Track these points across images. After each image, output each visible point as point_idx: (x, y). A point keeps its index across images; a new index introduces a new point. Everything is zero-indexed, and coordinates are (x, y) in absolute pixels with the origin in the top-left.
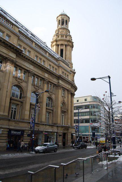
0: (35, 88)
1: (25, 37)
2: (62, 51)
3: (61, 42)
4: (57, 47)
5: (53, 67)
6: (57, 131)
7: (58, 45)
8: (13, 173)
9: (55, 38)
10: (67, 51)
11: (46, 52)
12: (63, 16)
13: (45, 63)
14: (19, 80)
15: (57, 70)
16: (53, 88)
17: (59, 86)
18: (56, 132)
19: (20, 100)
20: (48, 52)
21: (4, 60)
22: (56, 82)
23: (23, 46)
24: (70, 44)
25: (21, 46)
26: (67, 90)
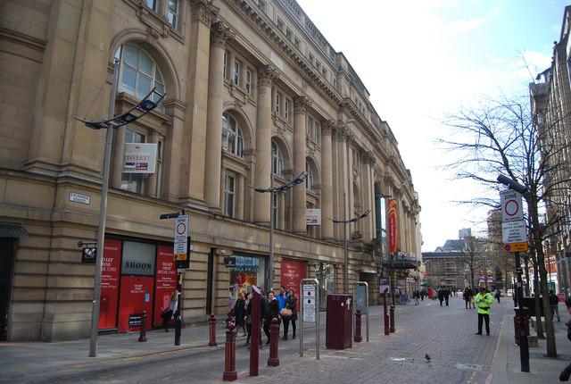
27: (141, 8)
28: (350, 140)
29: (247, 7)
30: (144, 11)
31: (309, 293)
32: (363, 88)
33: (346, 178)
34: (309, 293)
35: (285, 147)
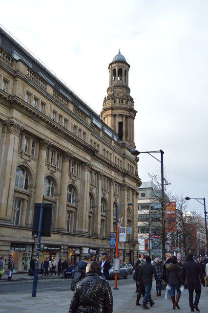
1: (35, 76)
2: (121, 124)
3: (119, 111)
4: (113, 118)
5: (60, 116)
6: (124, 248)
7: (114, 116)
8: (150, 290)
9: (109, 104)
10: (129, 127)
12: (121, 64)
13: (45, 108)
17: (12, 125)
18: (122, 250)
21: (36, 142)
23: (59, 112)
24: (131, 113)
25: (30, 95)
26: (132, 189)
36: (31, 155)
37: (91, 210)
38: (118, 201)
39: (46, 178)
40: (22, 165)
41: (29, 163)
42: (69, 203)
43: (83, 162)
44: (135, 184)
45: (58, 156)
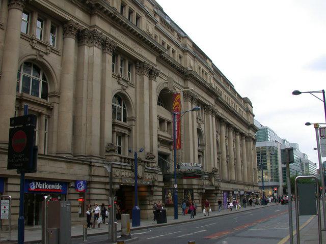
0: (119, 84)
11: (172, 30)
14: (123, 83)
15: (182, 59)
16: (121, 66)
19: (125, 123)
20: (176, 32)
22: (85, 24)
27: (32, 40)
28: (213, 112)
29: (120, 21)
30: (34, 41)
31: (5, 207)
32: (206, 57)
33: (147, 130)
34: (5, 207)
35: (130, 104)
36: (128, 79)
37: (200, 148)
38: (202, 126)
39: (115, 96)
40: (34, 60)
41: (45, 56)
42: (161, 133)
43: (66, 21)
44: (155, 58)
45: (121, 61)
